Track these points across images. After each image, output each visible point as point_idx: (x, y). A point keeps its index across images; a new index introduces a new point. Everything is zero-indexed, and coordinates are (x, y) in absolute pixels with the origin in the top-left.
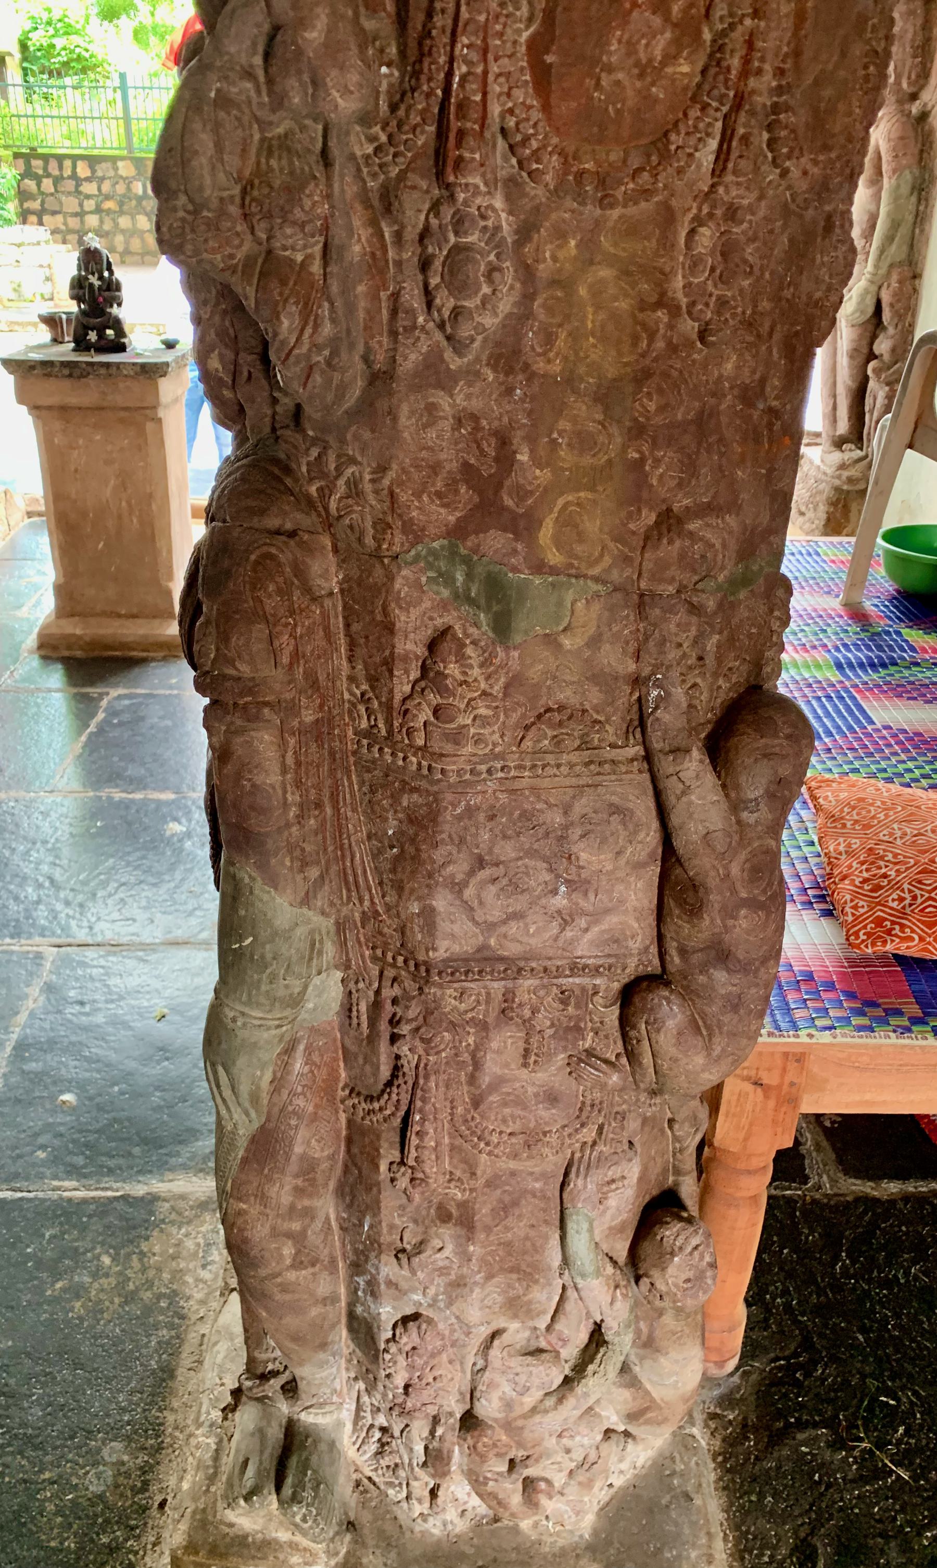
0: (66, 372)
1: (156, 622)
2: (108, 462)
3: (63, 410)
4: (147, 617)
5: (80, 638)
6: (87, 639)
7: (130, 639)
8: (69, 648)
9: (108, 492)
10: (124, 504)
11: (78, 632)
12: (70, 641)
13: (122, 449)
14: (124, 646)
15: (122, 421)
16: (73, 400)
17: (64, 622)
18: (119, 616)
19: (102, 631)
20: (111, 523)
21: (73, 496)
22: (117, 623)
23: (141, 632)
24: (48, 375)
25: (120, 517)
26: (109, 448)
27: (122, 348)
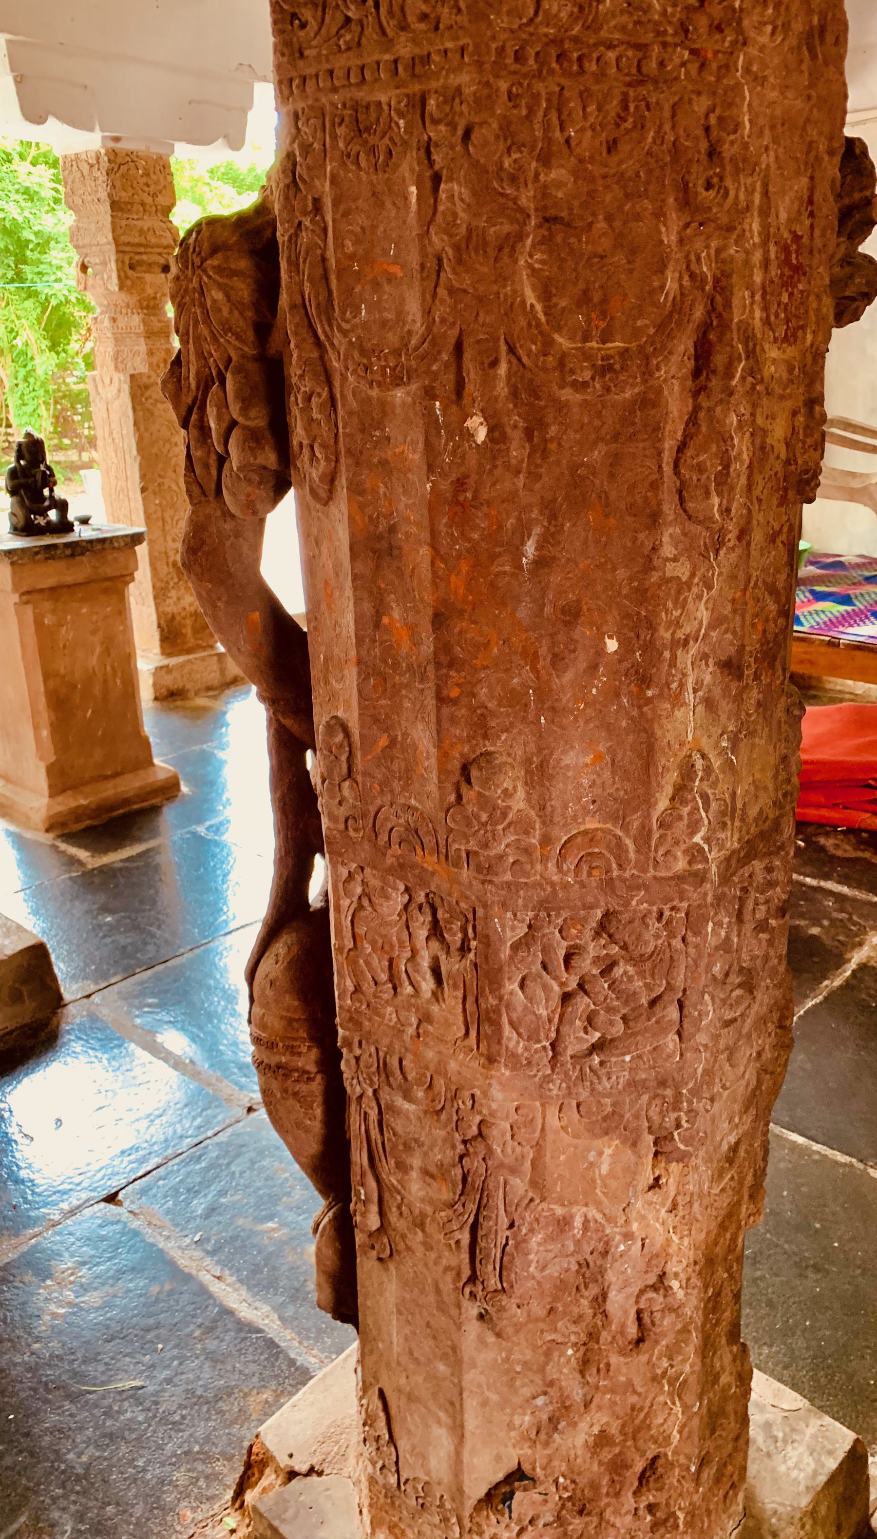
0: (68, 552)
1: (141, 773)
2: (94, 632)
3: (54, 592)
4: (131, 771)
5: (85, 807)
6: (93, 806)
7: (131, 793)
8: (78, 820)
9: (94, 661)
10: (109, 668)
11: (83, 802)
12: (77, 814)
13: (106, 617)
14: (127, 802)
15: (106, 591)
16: (69, 579)
17: (60, 799)
18: (106, 778)
19: (104, 795)
20: (97, 690)
21: (62, 671)
22: (110, 784)
23: (137, 784)
24: (53, 558)
25: (105, 681)
26: (95, 618)
27: (65, 527)
